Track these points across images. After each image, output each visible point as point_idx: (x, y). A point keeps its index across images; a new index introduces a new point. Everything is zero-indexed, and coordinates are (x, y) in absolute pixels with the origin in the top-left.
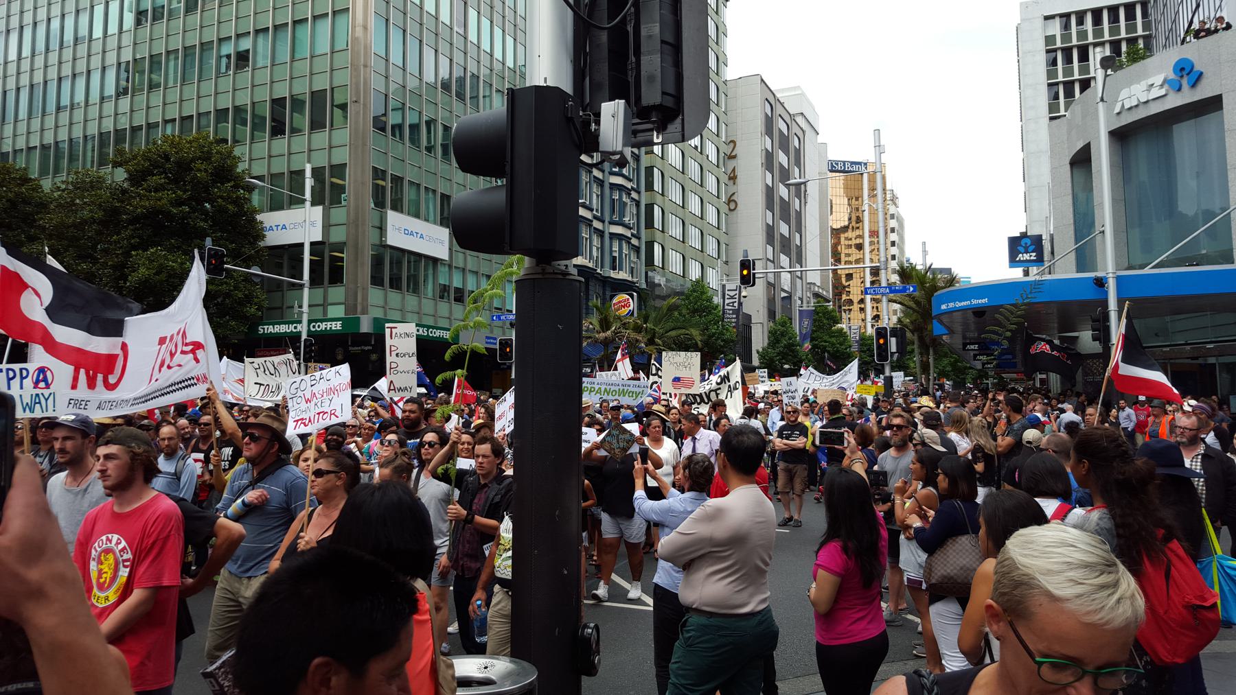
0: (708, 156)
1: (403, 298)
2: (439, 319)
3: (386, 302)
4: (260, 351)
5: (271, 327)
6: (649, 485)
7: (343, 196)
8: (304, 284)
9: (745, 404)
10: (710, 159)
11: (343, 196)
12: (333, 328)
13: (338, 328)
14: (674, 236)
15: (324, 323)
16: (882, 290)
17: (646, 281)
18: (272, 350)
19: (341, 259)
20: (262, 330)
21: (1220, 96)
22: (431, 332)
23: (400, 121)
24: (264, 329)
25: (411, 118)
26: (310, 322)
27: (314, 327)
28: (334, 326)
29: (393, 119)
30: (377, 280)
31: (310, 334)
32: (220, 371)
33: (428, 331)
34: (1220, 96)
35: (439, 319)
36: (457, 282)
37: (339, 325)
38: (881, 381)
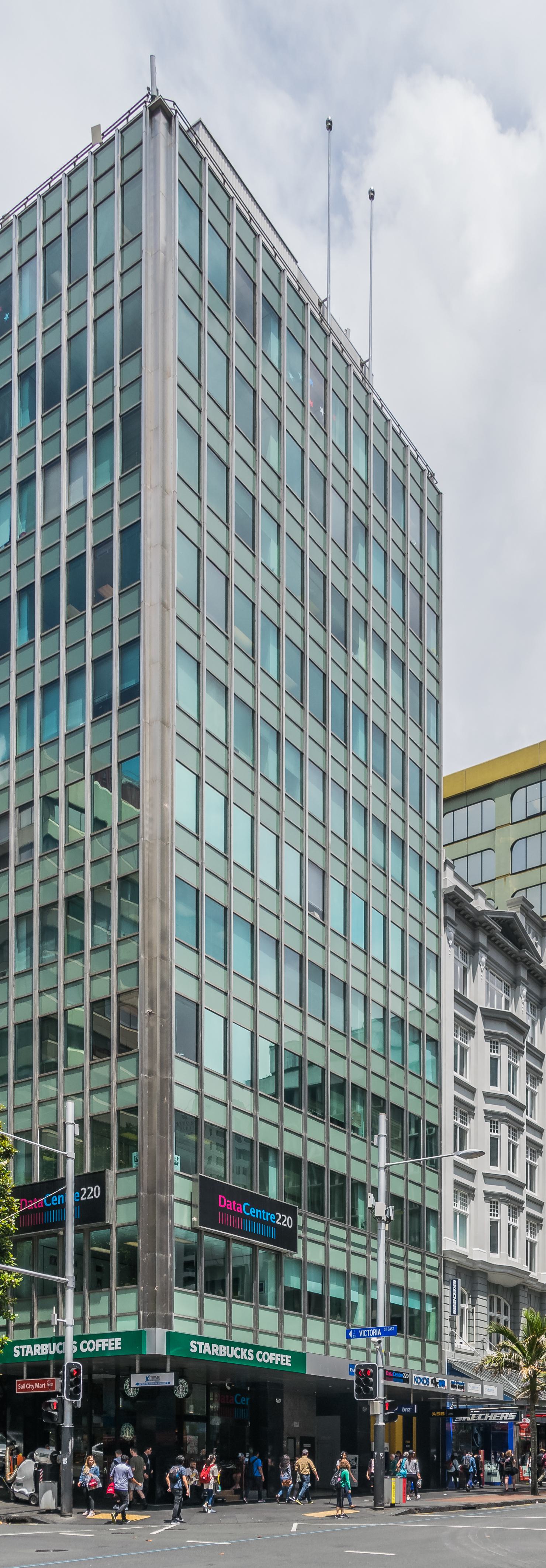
2: (285, 1341)
4: (22, 1383)
5: (30, 1346)
6: (56, 1484)
7: (134, 1154)
8: (66, 1283)
11: (134, 1154)
12: (110, 1348)
13: (117, 1348)
15: (98, 1341)
16: (143, 1075)
17: (452, 1284)
18: (37, 1382)
19: (135, 1249)
20: (18, 1352)
21: (99, 125)
22: (261, 1356)
24: (20, 1350)
26: (78, 1339)
27: (85, 1346)
28: (111, 1344)
29: (290, 1081)
30: (188, 1282)
31: (77, 1356)
32: (375, 1461)
33: (255, 1354)
34: (99, 125)
35: (285, 1341)
37: (117, 1344)
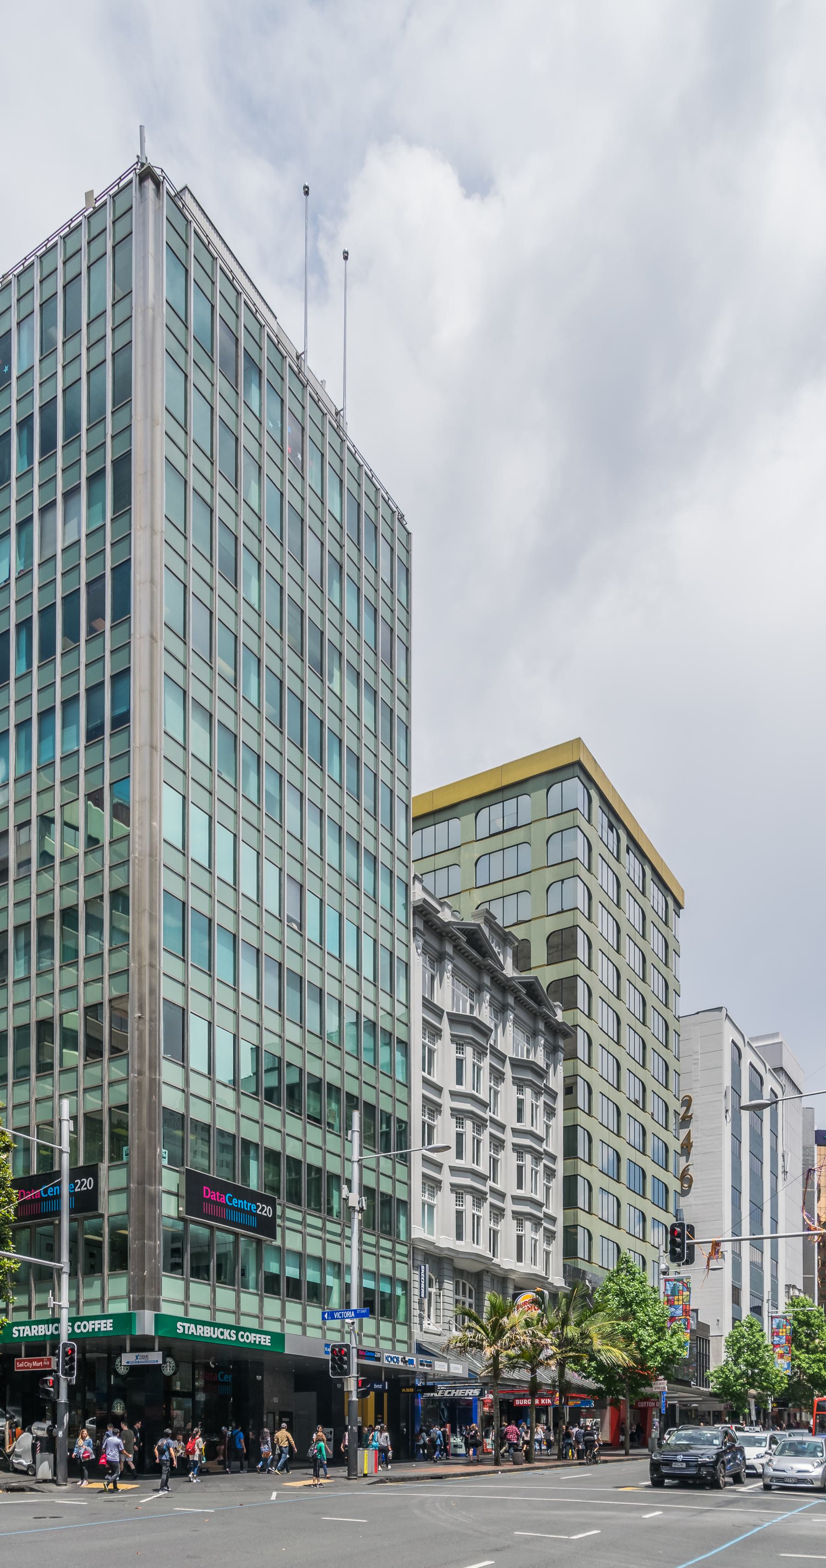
0: (652, 1114)
1: (214, 1291)
3: (187, 1296)
4: (20, 1362)
5: (27, 1328)
7: (125, 1148)
8: (61, 1268)
9: (183, 1468)
10: (656, 1117)
11: (125, 1148)
12: (103, 1329)
13: (109, 1329)
14: (605, 1218)
15: (91, 1322)
18: (35, 1360)
20: (17, 1333)
22: (242, 1336)
23: (276, 1084)
24: (19, 1331)
25: (291, 1077)
27: (79, 1327)
28: (103, 1325)
29: (269, 1081)
33: (237, 1335)
36: (292, 1272)
37: (109, 1325)
38: (164, 1196)
